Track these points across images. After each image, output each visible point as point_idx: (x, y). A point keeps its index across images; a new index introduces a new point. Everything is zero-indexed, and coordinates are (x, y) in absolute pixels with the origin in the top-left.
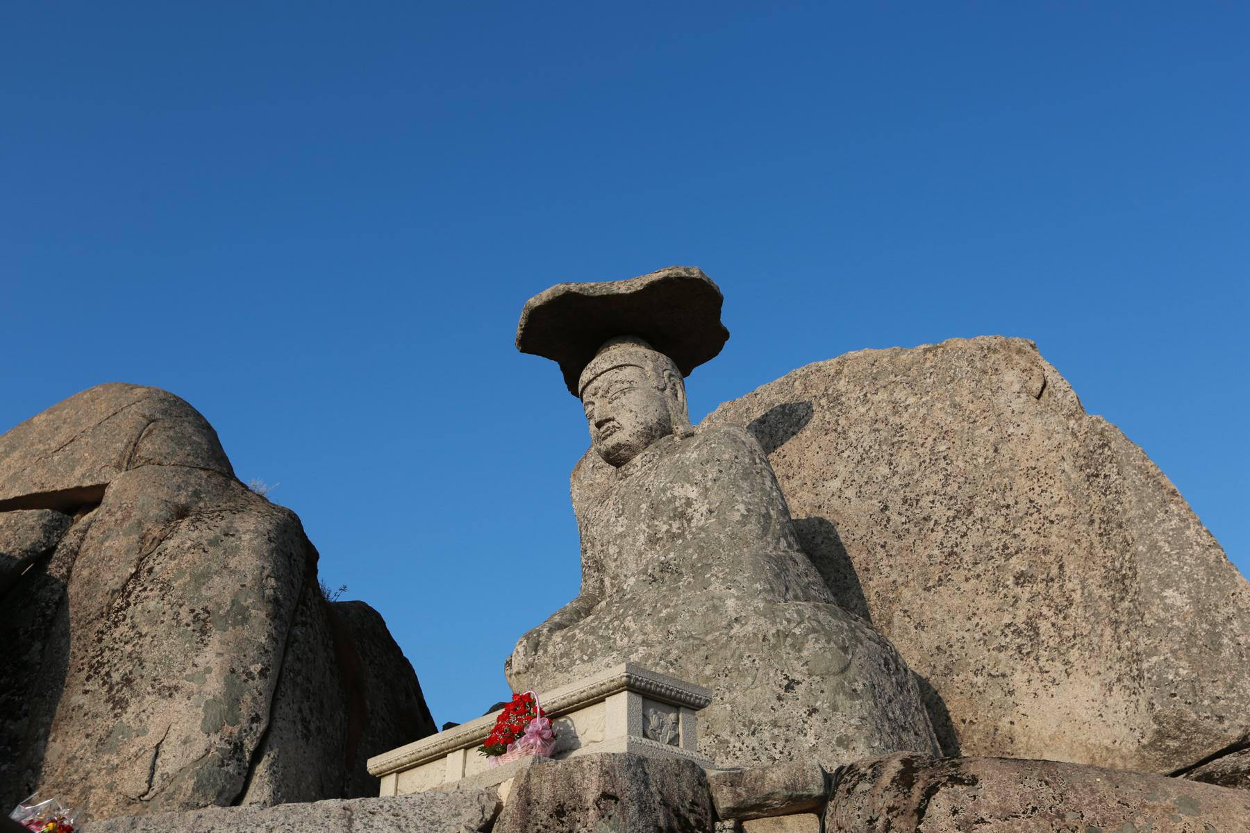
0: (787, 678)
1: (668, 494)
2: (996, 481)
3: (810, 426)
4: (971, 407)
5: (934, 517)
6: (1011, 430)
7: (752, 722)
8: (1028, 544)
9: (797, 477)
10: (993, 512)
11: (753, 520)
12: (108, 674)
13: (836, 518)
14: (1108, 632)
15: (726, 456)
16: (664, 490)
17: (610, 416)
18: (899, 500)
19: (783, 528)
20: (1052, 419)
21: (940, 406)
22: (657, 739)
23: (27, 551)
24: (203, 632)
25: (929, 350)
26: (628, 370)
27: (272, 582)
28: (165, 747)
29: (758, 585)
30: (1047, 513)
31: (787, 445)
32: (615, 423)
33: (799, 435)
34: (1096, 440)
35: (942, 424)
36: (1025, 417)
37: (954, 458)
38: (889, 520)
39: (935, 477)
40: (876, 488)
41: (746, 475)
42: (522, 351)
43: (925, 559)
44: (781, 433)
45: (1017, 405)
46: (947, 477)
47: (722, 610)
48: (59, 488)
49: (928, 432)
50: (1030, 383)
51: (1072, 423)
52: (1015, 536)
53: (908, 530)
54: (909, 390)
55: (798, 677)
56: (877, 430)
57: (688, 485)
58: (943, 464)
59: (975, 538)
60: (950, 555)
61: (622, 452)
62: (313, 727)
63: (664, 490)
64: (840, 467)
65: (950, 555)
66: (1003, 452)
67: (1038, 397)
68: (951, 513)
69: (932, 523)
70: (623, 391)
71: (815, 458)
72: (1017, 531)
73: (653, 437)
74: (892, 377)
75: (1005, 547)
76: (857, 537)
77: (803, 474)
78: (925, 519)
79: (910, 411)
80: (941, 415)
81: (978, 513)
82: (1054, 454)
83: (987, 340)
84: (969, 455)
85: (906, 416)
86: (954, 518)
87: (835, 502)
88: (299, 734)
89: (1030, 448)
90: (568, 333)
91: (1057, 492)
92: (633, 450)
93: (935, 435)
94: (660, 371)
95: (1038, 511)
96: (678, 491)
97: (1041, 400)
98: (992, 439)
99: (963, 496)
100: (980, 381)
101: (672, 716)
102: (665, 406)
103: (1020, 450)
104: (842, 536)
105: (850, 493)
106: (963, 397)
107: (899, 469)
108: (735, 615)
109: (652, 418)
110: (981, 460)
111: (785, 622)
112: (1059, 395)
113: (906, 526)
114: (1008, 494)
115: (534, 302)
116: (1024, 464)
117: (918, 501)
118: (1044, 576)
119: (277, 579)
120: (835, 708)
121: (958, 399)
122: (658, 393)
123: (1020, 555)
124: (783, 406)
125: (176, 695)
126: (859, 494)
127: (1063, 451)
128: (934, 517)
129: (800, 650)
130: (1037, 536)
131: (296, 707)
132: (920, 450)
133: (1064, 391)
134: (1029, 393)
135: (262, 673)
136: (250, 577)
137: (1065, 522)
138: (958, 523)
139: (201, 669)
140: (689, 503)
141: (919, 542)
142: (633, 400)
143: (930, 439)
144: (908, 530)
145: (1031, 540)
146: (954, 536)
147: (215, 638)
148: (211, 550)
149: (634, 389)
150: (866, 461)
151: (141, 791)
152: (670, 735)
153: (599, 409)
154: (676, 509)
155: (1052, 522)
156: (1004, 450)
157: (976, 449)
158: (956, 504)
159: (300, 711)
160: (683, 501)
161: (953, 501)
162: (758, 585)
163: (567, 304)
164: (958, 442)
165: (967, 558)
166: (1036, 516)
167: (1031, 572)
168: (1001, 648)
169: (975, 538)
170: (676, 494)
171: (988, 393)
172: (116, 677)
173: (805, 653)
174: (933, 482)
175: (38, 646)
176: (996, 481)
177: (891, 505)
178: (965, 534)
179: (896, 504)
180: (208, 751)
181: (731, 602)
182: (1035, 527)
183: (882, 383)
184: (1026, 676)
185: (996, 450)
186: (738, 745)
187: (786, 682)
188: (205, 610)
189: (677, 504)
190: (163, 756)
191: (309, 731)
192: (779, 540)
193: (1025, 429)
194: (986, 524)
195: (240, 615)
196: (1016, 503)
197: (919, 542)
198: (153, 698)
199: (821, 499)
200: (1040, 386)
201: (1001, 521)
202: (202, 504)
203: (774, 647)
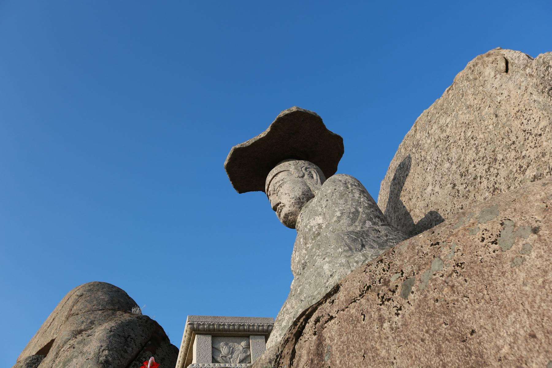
1: (308, 227)
2: (502, 133)
3: (412, 167)
4: (476, 102)
5: (479, 175)
6: (499, 99)
8: (532, 157)
9: (414, 197)
10: (507, 151)
11: (345, 217)
13: (436, 207)
15: (329, 191)
16: (306, 226)
17: (278, 202)
18: (458, 177)
19: (368, 215)
20: (517, 77)
21: (460, 113)
22: (226, 362)
25: (450, 89)
26: (280, 175)
27: (106, 352)
29: (340, 250)
30: (536, 132)
31: (406, 183)
32: (282, 205)
33: (409, 174)
34: (543, 69)
35: (465, 121)
36: (504, 87)
37: (477, 135)
38: (458, 191)
39: (471, 152)
40: (446, 177)
41: (342, 196)
42: (240, 193)
44: (402, 178)
45: (496, 84)
47: (322, 274)
49: (460, 130)
50: (498, 66)
51: (528, 70)
52: (524, 157)
53: (469, 191)
54: (446, 116)
56: (438, 146)
57: (317, 217)
58: (472, 142)
59: (503, 173)
60: (494, 191)
61: (290, 218)
63: (306, 226)
64: (429, 179)
65: (494, 191)
66: (500, 114)
67: (507, 71)
68: (486, 167)
69: (479, 178)
70: (280, 186)
71: (418, 181)
73: (303, 203)
74: (437, 115)
75: (521, 167)
76: (449, 211)
77: (416, 193)
78: (475, 179)
79: (449, 126)
80: (464, 117)
81: (500, 157)
82: (526, 95)
83: (470, 64)
84: (484, 128)
85: (448, 130)
86: (489, 169)
87: (433, 198)
89: (512, 102)
90: (249, 170)
91: (536, 114)
92: (294, 214)
93: (464, 129)
94: (299, 168)
95: (531, 134)
96: (313, 223)
97: (509, 72)
98: (492, 111)
99: (489, 154)
100: (475, 85)
101: (243, 344)
102: (306, 184)
103: (508, 106)
104: (442, 215)
105: (437, 189)
106: (470, 100)
107: (454, 160)
108: (330, 273)
109: (298, 193)
110: (491, 127)
111: (355, 264)
112: (516, 62)
113: (467, 189)
114: (511, 135)
115: (226, 163)
116: (513, 113)
117: (467, 171)
118: (547, 170)
119: (109, 350)
121: (468, 103)
122: (300, 179)
123: (530, 167)
124: (400, 165)
126: (441, 187)
127: (530, 90)
128: (479, 175)
130: (535, 149)
132: (460, 142)
133: (516, 57)
134: (500, 73)
136: (92, 353)
137: (547, 129)
138: (492, 170)
141: (477, 194)
142: (286, 188)
143: (462, 134)
144: (469, 191)
145: (532, 153)
146: (492, 179)
149: (285, 182)
150: (438, 166)
152: (241, 356)
153: (274, 200)
154: (314, 233)
155: (540, 135)
156: (501, 113)
157: (486, 122)
158: (487, 160)
160: (317, 227)
161: (485, 160)
162: (340, 250)
163: (239, 156)
164: (475, 125)
165: (503, 187)
166: (530, 138)
167: (539, 172)
169: (503, 173)
170: (312, 225)
171: (481, 88)
174: (471, 155)
176: (502, 133)
177: (456, 182)
178: (498, 174)
181: (326, 267)
182: (532, 145)
183: (433, 121)
185: (496, 116)
189: (314, 230)
192: (365, 222)
193: (506, 93)
194: (506, 161)
196: (517, 138)
197: (477, 194)
199: (426, 201)
200: (504, 64)
201: (513, 153)
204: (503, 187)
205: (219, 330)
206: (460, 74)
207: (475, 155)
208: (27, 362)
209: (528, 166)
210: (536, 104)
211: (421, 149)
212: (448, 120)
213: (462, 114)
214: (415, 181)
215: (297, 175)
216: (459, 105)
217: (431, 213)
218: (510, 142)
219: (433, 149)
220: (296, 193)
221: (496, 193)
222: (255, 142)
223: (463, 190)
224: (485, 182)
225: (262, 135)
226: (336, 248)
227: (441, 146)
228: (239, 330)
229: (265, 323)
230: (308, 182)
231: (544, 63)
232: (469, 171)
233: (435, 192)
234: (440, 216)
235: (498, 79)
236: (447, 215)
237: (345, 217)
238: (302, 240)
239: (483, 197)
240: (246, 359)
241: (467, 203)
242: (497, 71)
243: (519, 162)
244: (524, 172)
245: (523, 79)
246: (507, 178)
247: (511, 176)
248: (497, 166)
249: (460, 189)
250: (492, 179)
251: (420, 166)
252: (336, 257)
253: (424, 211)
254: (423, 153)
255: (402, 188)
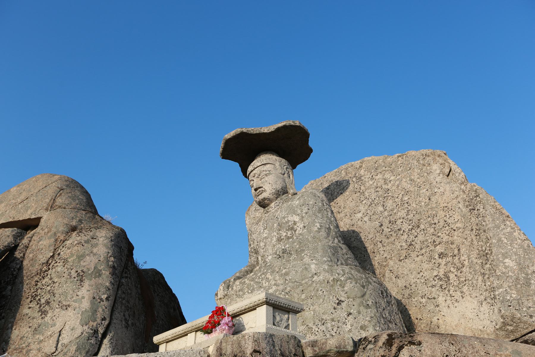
0: (338, 299)
2: (430, 212)
3: (348, 190)
4: (418, 180)
5: (403, 229)
6: (436, 190)
7: (323, 319)
9: (343, 212)
10: (429, 226)
11: (323, 230)
12: (39, 300)
13: (360, 230)
14: (480, 278)
15: (311, 203)
16: (284, 218)
17: (261, 186)
20: (454, 185)
21: (405, 180)
23: (6, 246)
24: (81, 281)
25: (400, 156)
26: (268, 166)
27: (112, 259)
28: (63, 332)
30: (452, 227)
31: (338, 199)
32: (263, 189)
33: (344, 194)
36: (442, 184)
37: (411, 203)
38: (383, 230)
39: (403, 211)
40: (377, 216)
41: (320, 211)
43: (399, 247)
44: (336, 193)
45: (438, 179)
46: (408, 211)
48: (21, 219)
49: (400, 192)
50: (444, 169)
51: (463, 187)
52: (438, 237)
53: (391, 235)
54: (391, 174)
55: (343, 299)
57: (294, 216)
58: (406, 205)
59: (421, 238)
60: (410, 245)
61: (266, 201)
62: (130, 323)
63: (284, 218)
65: (410, 245)
66: (433, 200)
67: (448, 176)
68: (410, 227)
69: (402, 231)
70: (266, 175)
72: (439, 234)
73: (280, 195)
74: (384, 168)
75: (434, 241)
76: (369, 238)
78: (399, 230)
79: (392, 183)
80: (406, 184)
81: (422, 227)
82: (455, 200)
85: (390, 185)
86: (412, 229)
87: (360, 223)
88: (123, 326)
89: (444, 198)
90: (243, 150)
91: (457, 217)
92: (271, 201)
93: (403, 193)
96: (290, 218)
98: (428, 194)
99: (415, 220)
100: (422, 169)
101: (286, 316)
102: (284, 181)
104: (363, 238)
105: (366, 219)
106: (415, 177)
107: (387, 208)
109: (279, 187)
110: (423, 204)
111: (337, 275)
112: (457, 175)
113: (391, 233)
114: (435, 218)
115: (228, 136)
117: (396, 222)
119: (114, 258)
120: (359, 313)
121: (412, 177)
122: (282, 176)
123: (441, 245)
124: (337, 182)
125: (69, 309)
126: (370, 220)
128: (403, 229)
129: (343, 287)
131: (122, 314)
132: (396, 200)
134: (444, 174)
135: (107, 299)
136: (102, 257)
137: (460, 230)
138: (413, 231)
139: (80, 297)
140: (295, 223)
143: (401, 195)
144: (391, 235)
145: (445, 238)
146: (412, 237)
147: (87, 283)
148: (86, 245)
149: (271, 174)
150: (373, 205)
151: (52, 351)
153: (256, 183)
154: (289, 226)
155: (455, 230)
157: (421, 199)
159: (124, 315)
160: (293, 222)
161: (411, 222)
163: (242, 137)
164: (413, 196)
165: (418, 246)
166: (447, 228)
168: (433, 286)
169: (421, 238)
170: (289, 219)
171: (426, 174)
172: (43, 301)
173: (346, 288)
174: (402, 213)
175: (9, 287)
176: (430, 212)
177: (384, 224)
179: (386, 223)
180: (82, 333)
181: (313, 266)
183: (379, 171)
184: (444, 299)
185: (430, 199)
186: (317, 329)
187: (337, 301)
188: (82, 271)
189: (290, 224)
190: (62, 336)
191: (128, 324)
193: (442, 190)
194: (426, 232)
195: (98, 273)
196: (439, 222)
197: (396, 240)
198: (59, 310)
199: (353, 222)
200: (448, 171)
201: (432, 230)
202: (82, 225)
203: (332, 286)
204: (418, 246)
205: (278, 305)
206: (413, 153)
207: (405, 214)
208: (14, 233)
209: (439, 244)
210: (459, 210)
211: (362, 183)
212: (392, 178)
213: (405, 182)
214: (348, 202)
215: (280, 171)
216: (405, 174)
217: (354, 231)
218: (433, 222)
219: (373, 191)
220: (277, 186)
221: (411, 247)
222: (259, 133)
223: (387, 232)
224: (405, 236)
225: (266, 130)
226: (322, 256)
227: (380, 193)
228: (287, 308)
229: (300, 307)
230: (287, 180)
231: (476, 191)
232: (397, 223)
233: (363, 220)
234: (361, 238)
235: (440, 177)
236: (366, 240)
237: (323, 230)
238: (275, 225)
239: (400, 244)
240: (145, 263)
241: (387, 241)
242: (442, 172)
243: (434, 237)
244: (435, 246)
245: (457, 189)
246: (422, 242)
247: (426, 243)
248: (418, 230)
249: (384, 229)
250: (412, 237)
251: (356, 195)
252: (322, 263)
253: (348, 226)
254: (362, 188)
255: (333, 200)
